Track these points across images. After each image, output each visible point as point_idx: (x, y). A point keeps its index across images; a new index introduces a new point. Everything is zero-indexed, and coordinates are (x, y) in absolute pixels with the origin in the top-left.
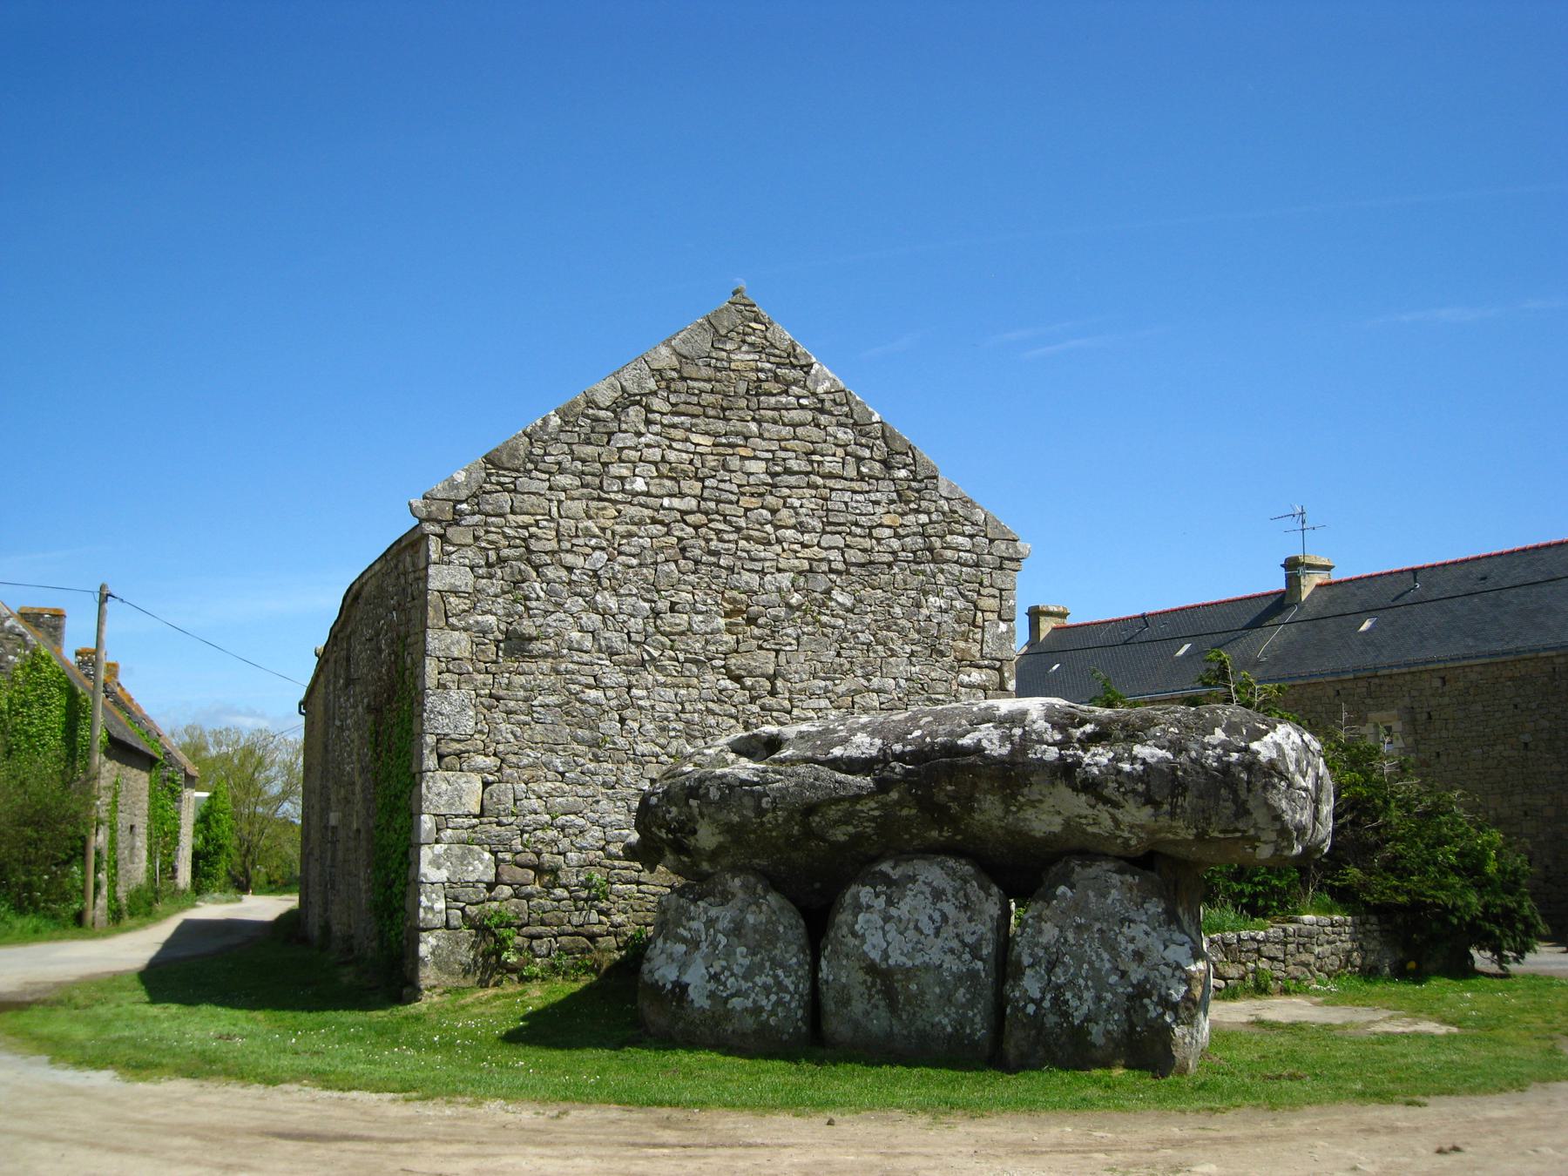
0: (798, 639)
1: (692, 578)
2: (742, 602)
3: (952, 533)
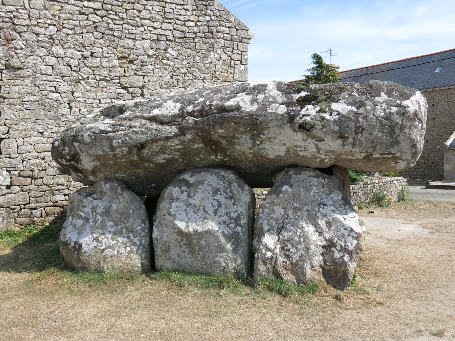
0: (153, 70)
1: (101, 41)
2: (125, 53)
3: (220, 25)
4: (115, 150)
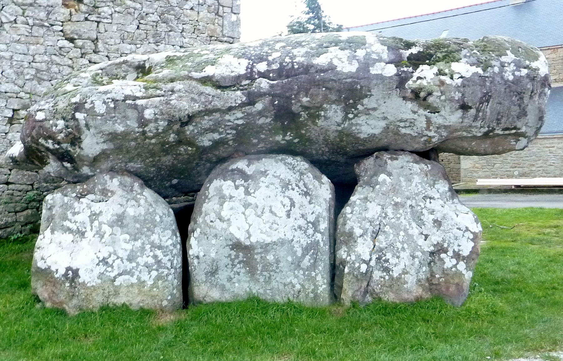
4: (146, 125)
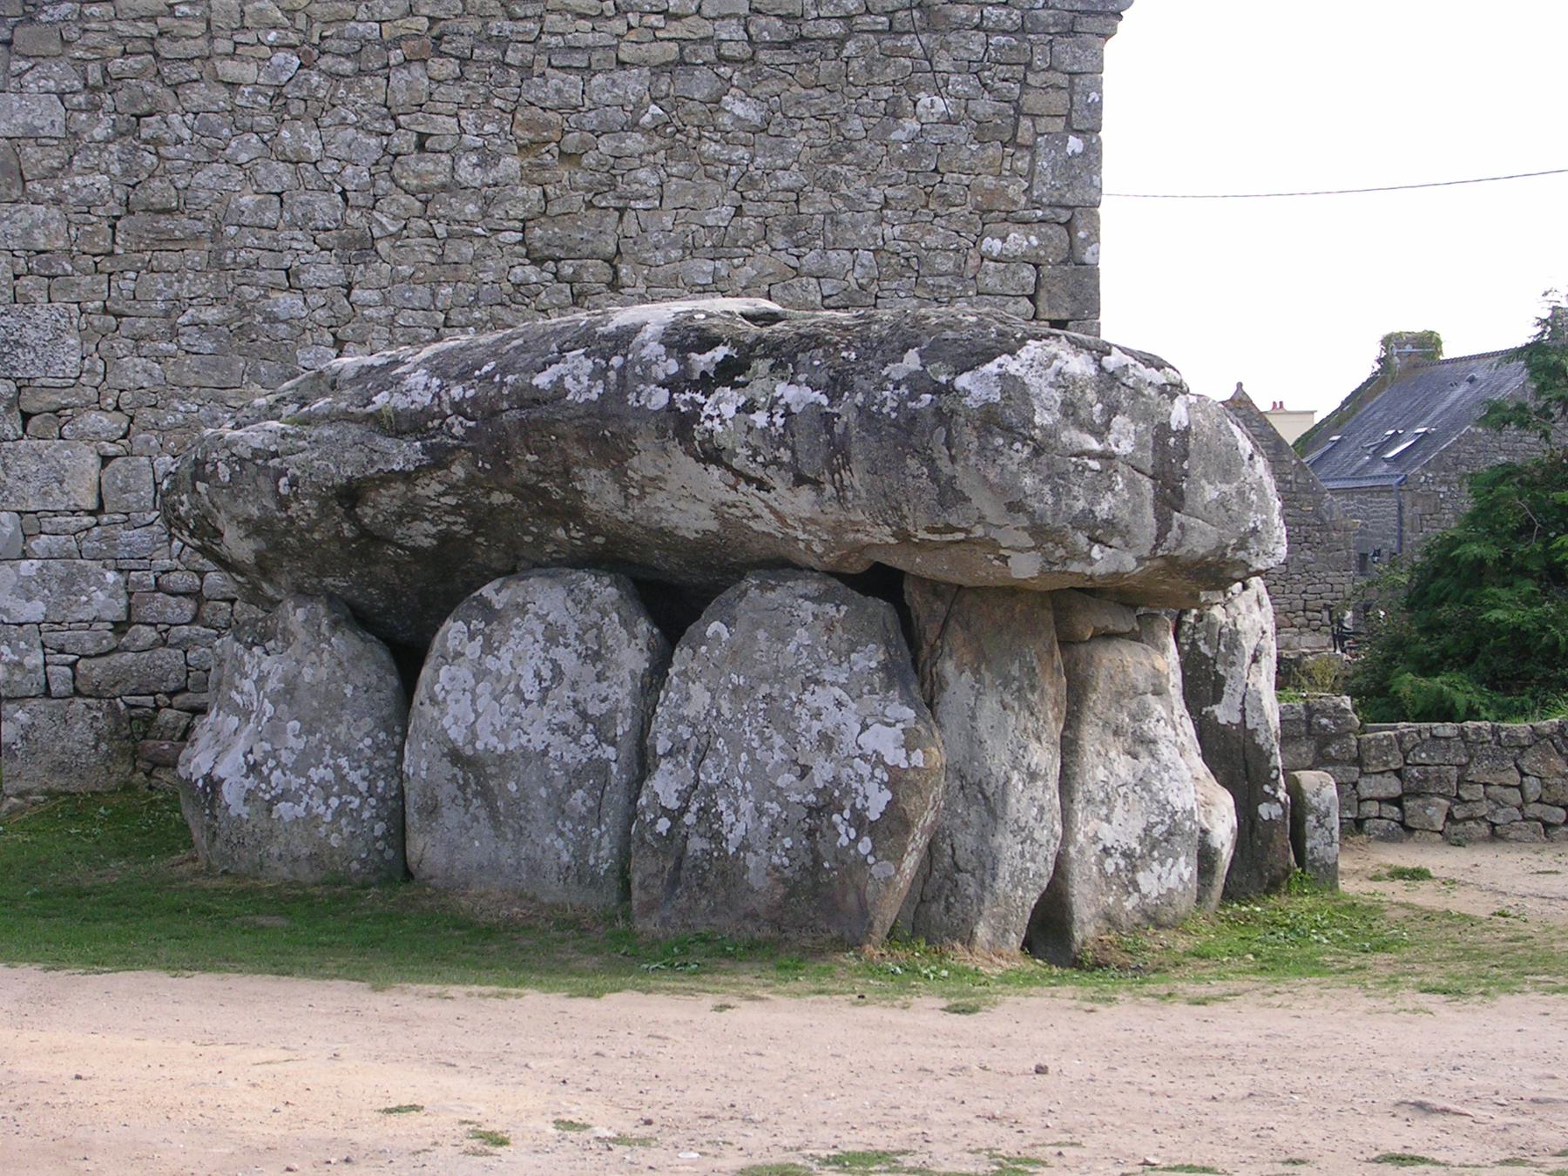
1: (459, 93)
2: (547, 125)
